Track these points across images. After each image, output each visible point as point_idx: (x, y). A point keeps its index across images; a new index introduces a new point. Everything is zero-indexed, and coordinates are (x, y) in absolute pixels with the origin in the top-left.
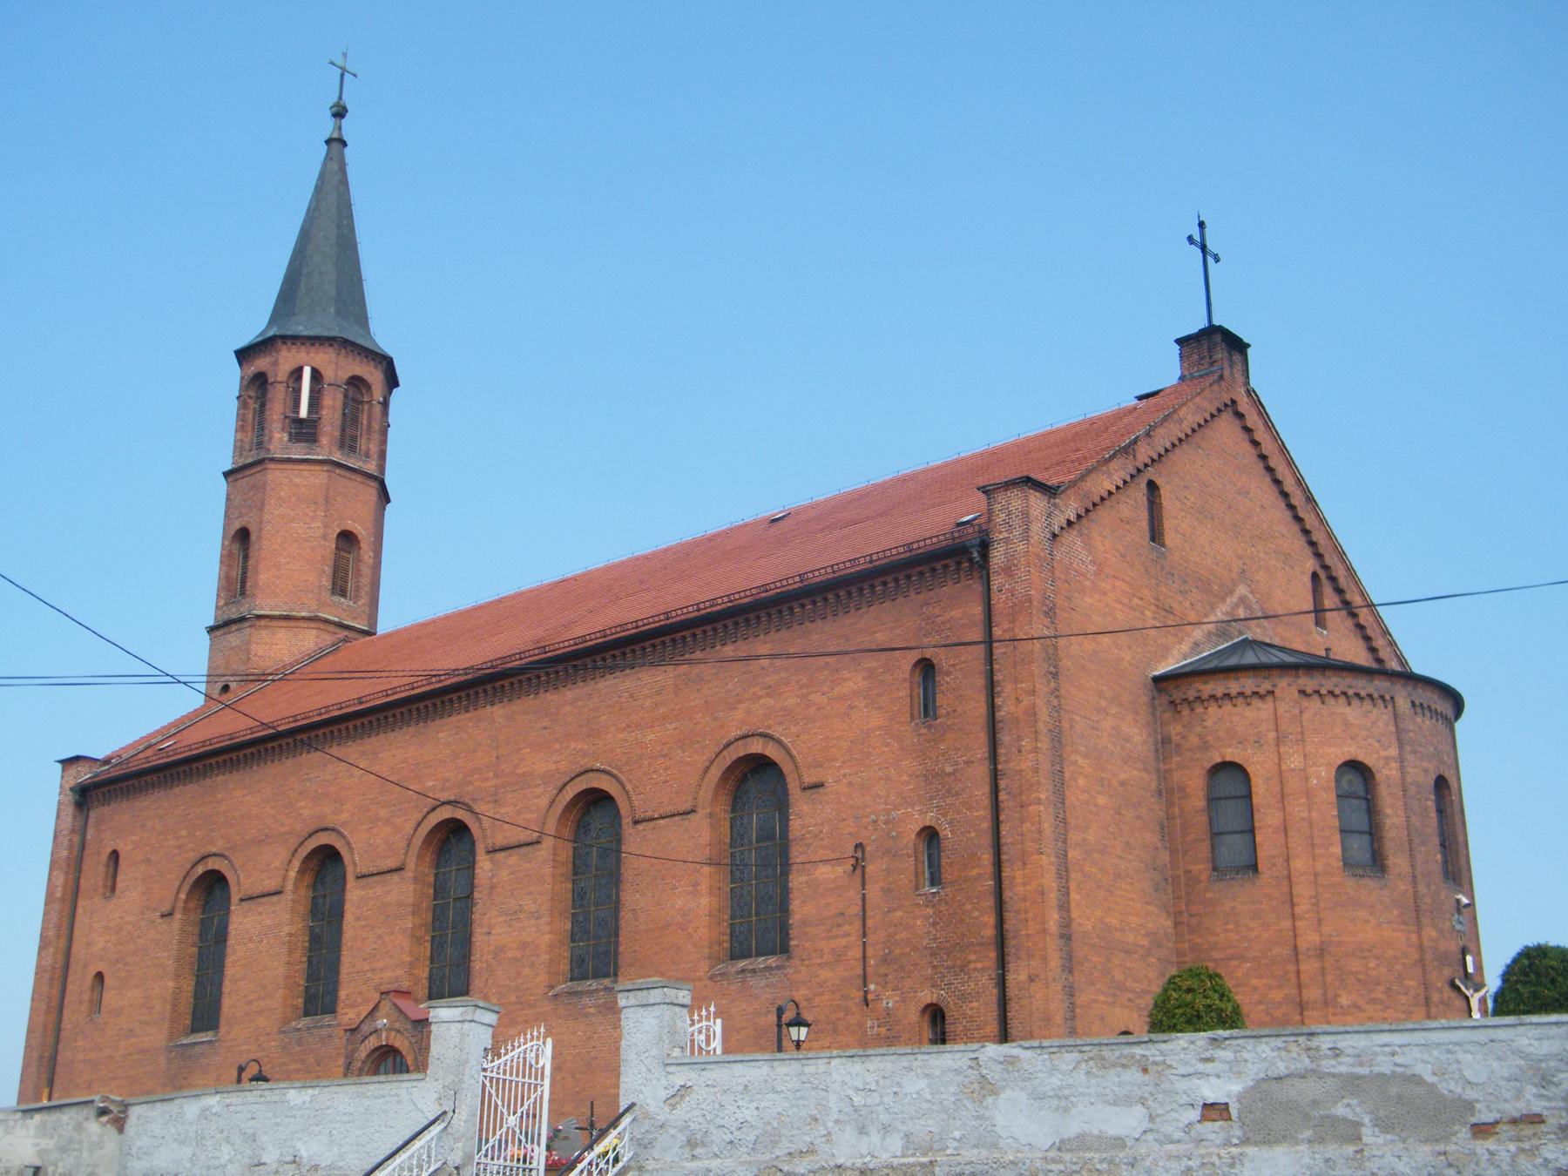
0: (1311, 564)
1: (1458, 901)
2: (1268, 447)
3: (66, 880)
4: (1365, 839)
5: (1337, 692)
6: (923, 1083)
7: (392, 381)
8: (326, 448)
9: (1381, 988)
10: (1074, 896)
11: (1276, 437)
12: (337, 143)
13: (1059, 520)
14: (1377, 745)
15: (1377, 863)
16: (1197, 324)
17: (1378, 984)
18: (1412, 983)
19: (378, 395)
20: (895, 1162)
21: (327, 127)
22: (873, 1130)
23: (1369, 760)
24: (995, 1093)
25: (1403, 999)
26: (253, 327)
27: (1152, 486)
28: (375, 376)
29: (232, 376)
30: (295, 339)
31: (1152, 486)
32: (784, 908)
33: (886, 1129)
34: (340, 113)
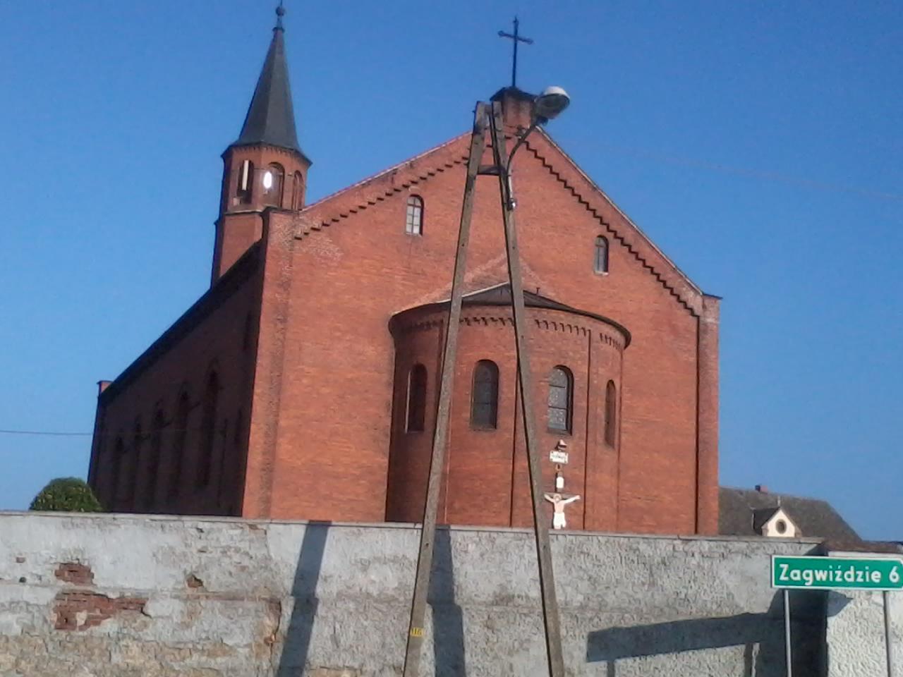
1: (559, 443)
5: (479, 318)
9: (481, 498)
12: (278, 30)
14: (503, 349)
17: (480, 495)
18: (504, 494)
21: (272, 21)
25: (496, 505)
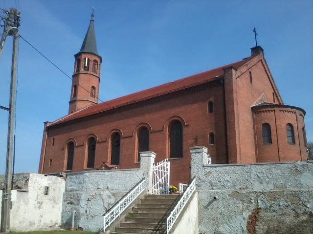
0: (272, 91)
2: (267, 69)
3: (9, 224)
4: (291, 138)
6: (279, 171)
7: (101, 61)
8: (90, 72)
10: (241, 146)
11: (268, 67)
13: (237, 76)
15: (294, 142)
16: (254, 46)
19: (99, 63)
20: (272, 191)
21: (90, 18)
22: (264, 183)
23: (292, 123)
24: (301, 173)
26: (78, 51)
27: (250, 73)
28: (98, 60)
29: (74, 59)
30: (83, 53)
31: (250, 73)
32: (182, 148)
33: (268, 183)
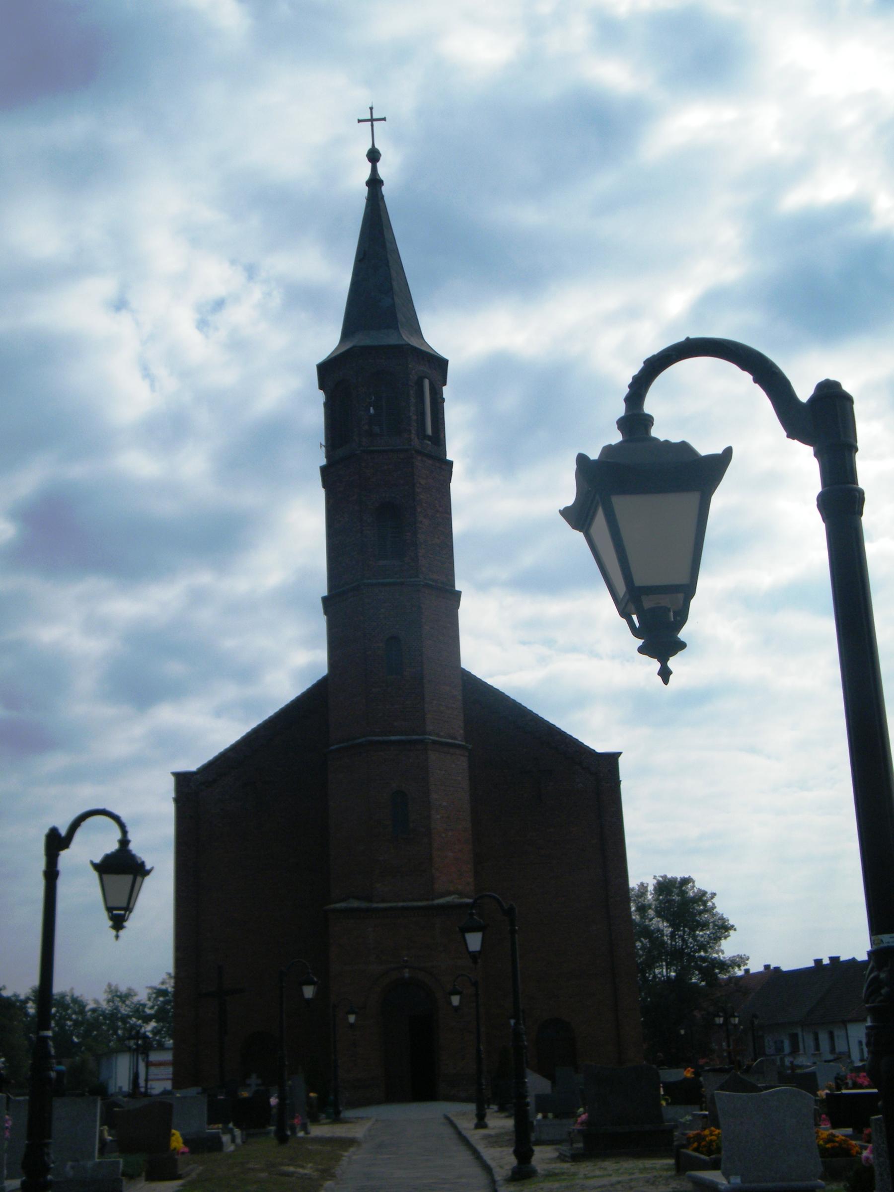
12: (375, 183)
34: (374, 156)
